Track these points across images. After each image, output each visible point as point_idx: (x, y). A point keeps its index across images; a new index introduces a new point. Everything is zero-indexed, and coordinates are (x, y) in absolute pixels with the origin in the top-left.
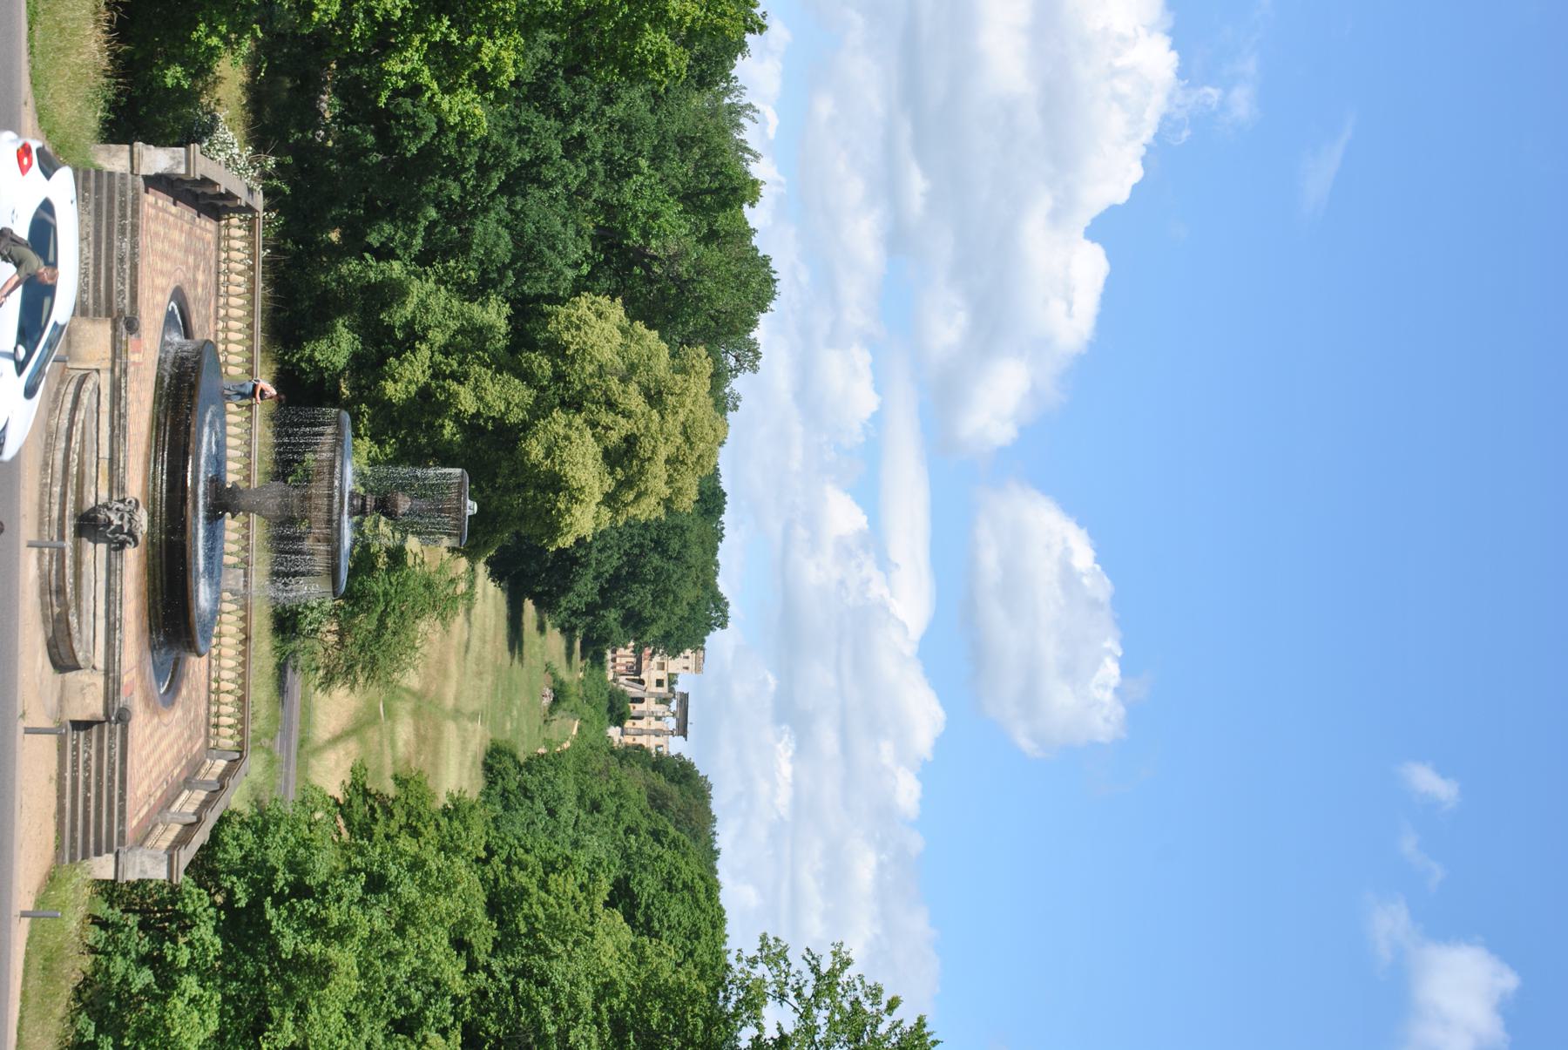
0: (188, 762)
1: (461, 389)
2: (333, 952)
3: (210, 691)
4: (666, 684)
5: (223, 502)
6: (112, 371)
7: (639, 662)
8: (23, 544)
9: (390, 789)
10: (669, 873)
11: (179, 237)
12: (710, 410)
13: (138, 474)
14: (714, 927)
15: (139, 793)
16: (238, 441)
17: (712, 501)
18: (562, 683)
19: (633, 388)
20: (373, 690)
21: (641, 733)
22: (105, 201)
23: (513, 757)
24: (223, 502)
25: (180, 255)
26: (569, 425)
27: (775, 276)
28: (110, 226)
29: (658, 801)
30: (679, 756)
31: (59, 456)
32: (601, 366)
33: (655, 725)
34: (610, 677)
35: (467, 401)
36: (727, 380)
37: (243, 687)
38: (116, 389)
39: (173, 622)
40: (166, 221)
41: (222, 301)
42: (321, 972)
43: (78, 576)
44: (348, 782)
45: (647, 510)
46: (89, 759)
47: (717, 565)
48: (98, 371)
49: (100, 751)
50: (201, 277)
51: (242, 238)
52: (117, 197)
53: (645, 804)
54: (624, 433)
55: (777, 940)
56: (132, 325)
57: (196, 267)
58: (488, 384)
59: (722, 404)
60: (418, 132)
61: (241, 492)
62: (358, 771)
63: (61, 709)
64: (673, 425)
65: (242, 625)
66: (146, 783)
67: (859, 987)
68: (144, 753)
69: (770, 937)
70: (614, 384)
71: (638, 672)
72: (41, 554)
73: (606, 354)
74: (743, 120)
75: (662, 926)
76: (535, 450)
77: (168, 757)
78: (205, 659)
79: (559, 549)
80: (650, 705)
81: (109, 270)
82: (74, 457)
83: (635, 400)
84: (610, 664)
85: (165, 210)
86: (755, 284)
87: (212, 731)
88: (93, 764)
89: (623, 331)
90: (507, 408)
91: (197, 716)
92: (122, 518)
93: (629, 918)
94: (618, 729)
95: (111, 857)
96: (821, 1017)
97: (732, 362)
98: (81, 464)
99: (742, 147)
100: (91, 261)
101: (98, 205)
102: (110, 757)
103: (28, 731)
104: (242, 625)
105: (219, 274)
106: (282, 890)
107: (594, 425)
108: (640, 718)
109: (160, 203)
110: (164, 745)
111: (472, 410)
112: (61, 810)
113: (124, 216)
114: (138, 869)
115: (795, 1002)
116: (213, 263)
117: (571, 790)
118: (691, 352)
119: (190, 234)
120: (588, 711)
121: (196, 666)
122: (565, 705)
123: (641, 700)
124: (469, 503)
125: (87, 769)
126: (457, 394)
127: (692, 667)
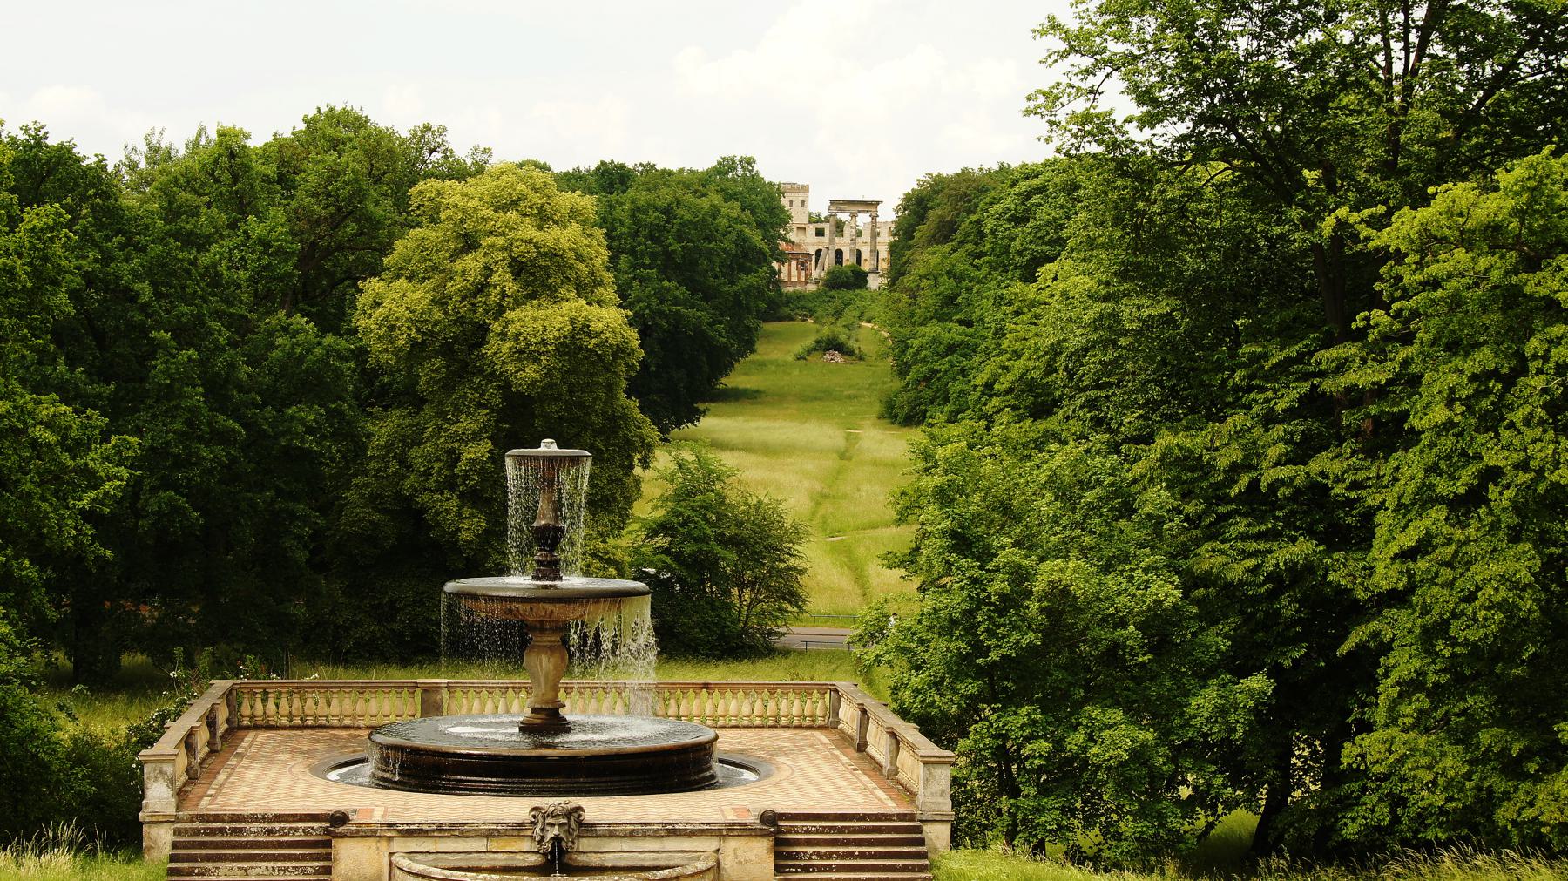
0: (838, 747)
1: (466, 456)
2: (1038, 587)
4: (820, 226)
7: (795, 256)
10: (1009, 221)
15: (860, 800)
17: (611, 179)
18: (819, 342)
21: (875, 253)
24: (549, 721)
26: (503, 336)
27: (324, 110)
29: (945, 232)
33: (866, 237)
34: (812, 288)
38: (410, 833)
39: (680, 768)
42: (1060, 597)
44: (903, 572)
46: (818, 854)
47: (681, 170)
48: (391, 854)
49: (809, 843)
51: (303, 700)
52: (199, 839)
53: (947, 248)
56: (340, 819)
58: (459, 428)
60: (176, 510)
62: (892, 560)
66: (849, 792)
70: (454, 287)
77: (827, 769)
79: (641, 346)
80: (844, 243)
81: (281, 845)
83: (471, 263)
84: (799, 288)
85: (222, 786)
86: (335, 131)
90: (485, 407)
92: (552, 825)
94: (870, 278)
95: (927, 828)
97: (436, 156)
100: (271, 864)
102: (817, 832)
106: (969, 644)
107: (501, 310)
108: (859, 253)
109: (211, 791)
110: (813, 774)
111: (489, 445)
113: (222, 831)
114: (940, 800)
115: (1101, 75)
116: (290, 733)
117: (933, 329)
118: (414, 202)
119: (253, 758)
120: (849, 315)
121: (727, 742)
122: (843, 338)
123: (839, 253)
125: (829, 856)
127: (801, 197)
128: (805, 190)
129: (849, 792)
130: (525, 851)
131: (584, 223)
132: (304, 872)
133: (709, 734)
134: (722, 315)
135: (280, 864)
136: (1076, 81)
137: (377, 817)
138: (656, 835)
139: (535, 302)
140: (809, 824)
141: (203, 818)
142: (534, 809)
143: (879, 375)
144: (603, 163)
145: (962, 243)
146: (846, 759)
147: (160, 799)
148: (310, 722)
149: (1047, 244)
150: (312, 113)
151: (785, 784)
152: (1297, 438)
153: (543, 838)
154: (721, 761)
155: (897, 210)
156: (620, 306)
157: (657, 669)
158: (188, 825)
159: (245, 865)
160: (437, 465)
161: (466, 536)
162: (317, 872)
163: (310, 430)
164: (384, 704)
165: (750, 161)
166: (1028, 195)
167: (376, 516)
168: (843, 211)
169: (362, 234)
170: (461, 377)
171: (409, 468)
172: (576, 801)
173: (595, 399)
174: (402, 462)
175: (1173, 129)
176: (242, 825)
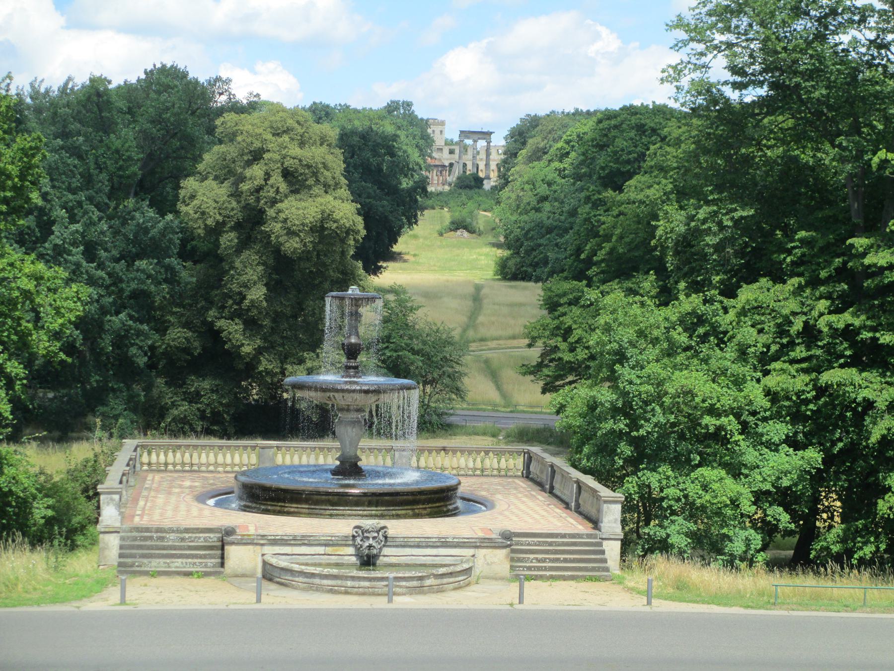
1: (249, 297)
3: (166, 471)
5: (350, 468)
6: (263, 545)
8: (390, 606)
11: (161, 499)
13: (341, 526)
14: (636, 114)
15: (559, 524)
16: (298, 459)
19: (248, 173)
20: (467, 359)
21: (487, 165)
22: (141, 552)
23: (507, 259)
24: (350, 468)
25: (173, 499)
27: (159, 65)
30: (506, 138)
31: (325, 582)
32: (232, 195)
33: (483, 155)
35: (257, 293)
36: (237, 102)
37: (478, 452)
39: (437, 501)
40: (151, 508)
41: (220, 469)
43: (408, 566)
44: (532, 377)
45: (336, 163)
46: (536, 559)
47: (364, 109)
50: (187, 483)
52: (137, 543)
54: (281, 179)
55: (663, 71)
56: (230, 532)
57: (181, 487)
59: (253, 107)
61: (342, 455)
63: (502, 579)
64: (273, 143)
65: (434, 453)
66: (551, 519)
67: (697, 11)
68: (531, 521)
69: (661, 75)
71: (444, 166)
72: (395, 594)
74: (42, 90)
75: (634, 152)
76: (292, 245)
77: (531, 504)
78: (462, 479)
80: (468, 159)
81: (190, 548)
82: (326, 571)
83: (257, 171)
85: (143, 509)
86: (166, 81)
87: (170, 467)
88: (540, 556)
89: (204, 179)
91: (500, 484)
93: (630, 175)
94: (485, 182)
95: (605, 543)
96: (719, 38)
98: (329, 565)
99: (63, 90)
100: (184, 560)
101: (144, 556)
102: (536, 545)
103: (521, 601)
104: (434, 453)
105: (192, 470)
107: (273, 202)
109: (138, 512)
112: (572, 578)
113: (151, 538)
114: (614, 525)
115: (710, 56)
116: (176, 475)
119: (157, 490)
121: (466, 486)
122: (468, 220)
123: (465, 165)
124: (350, 292)
126: (252, 301)
128: (442, 123)
129: (551, 519)
131: (329, 145)
132: (206, 566)
133: (453, 482)
134: (398, 206)
135: (190, 560)
136: (693, 60)
137: (252, 531)
139: (298, 196)
140: (530, 539)
141: (138, 529)
142: (356, 527)
144: (314, 103)
146: (542, 497)
149: (621, 164)
150: (149, 68)
151: (506, 513)
154: (464, 499)
156: (352, 201)
157: (418, 438)
158: (129, 534)
160: (230, 302)
163: (149, 276)
164: (239, 458)
165: (409, 105)
168: (468, 138)
169: (182, 148)
170: (246, 244)
172: (383, 523)
173: (333, 261)
174: (206, 300)
175: (751, 95)
176: (164, 535)
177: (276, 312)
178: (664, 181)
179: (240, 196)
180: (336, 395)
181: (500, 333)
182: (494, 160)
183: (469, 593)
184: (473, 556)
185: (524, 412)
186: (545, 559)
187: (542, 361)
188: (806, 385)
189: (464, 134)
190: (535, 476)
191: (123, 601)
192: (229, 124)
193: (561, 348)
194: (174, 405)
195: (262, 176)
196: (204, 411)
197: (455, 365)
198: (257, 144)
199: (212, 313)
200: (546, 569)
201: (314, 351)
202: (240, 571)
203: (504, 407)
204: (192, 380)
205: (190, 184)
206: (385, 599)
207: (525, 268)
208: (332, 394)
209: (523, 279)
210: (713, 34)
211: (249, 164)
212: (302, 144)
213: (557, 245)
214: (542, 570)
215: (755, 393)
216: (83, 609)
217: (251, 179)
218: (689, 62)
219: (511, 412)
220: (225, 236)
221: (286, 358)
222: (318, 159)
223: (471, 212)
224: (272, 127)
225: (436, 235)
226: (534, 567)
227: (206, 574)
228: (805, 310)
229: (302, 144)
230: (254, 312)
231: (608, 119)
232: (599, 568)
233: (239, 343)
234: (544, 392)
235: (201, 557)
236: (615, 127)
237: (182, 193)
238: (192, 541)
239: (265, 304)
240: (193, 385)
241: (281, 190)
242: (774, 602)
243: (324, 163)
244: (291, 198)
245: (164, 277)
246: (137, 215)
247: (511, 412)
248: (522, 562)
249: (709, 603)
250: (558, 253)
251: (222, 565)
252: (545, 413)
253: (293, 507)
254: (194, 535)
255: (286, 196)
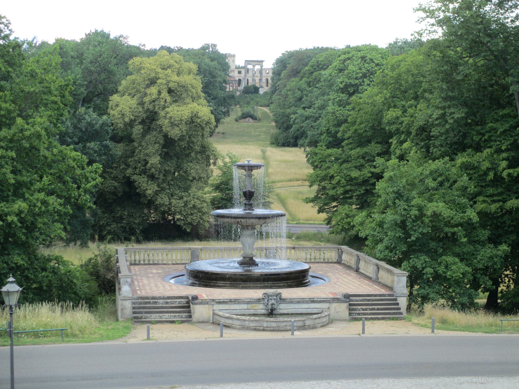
1: (150, 162)
8: (293, 337)
9: (315, 187)
12: (155, 57)
15: (371, 289)
22: (145, 310)
24: (249, 262)
27: (93, 31)
28: (154, 308)
33: (258, 74)
35: (155, 160)
39: (298, 279)
42: (435, 215)
46: (362, 309)
52: (142, 305)
53: (297, 79)
54: (167, 95)
56: (195, 298)
57: (152, 273)
64: (162, 74)
73: (133, 102)
76: (175, 133)
77: (349, 278)
81: (172, 307)
83: (153, 90)
86: (98, 39)
88: (364, 307)
92: (271, 299)
94: (260, 89)
100: (170, 315)
102: (360, 301)
103: (363, 333)
107: (164, 108)
112: (383, 319)
113: (149, 303)
122: (252, 112)
125: (366, 309)
126: (152, 164)
128: (234, 56)
130: (261, 308)
132: (182, 317)
133: (306, 266)
135: (172, 314)
136: (429, 28)
138: (307, 302)
139: (177, 104)
140: (357, 298)
141: (142, 298)
143: (270, 127)
145: (302, 77)
146: (354, 274)
147: (126, 292)
148: (151, 262)
151: (339, 283)
152: (511, 158)
153: (268, 304)
154: (313, 277)
155: (273, 64)
158: (137, 301)
159: (161, 315)
160: (139, 165)
161: (149, 192)
162: (186, 317)
163: (95, 152)
165: (215, 46)
166: (345, 61)
167: (116, 184)
168: (250, 64)
170: (148, 132)
171: (128, 166)
172: (279, 291)
174: (125, 164)
176: (156, 300)
177: (165, 170)
178: (385, 91)
179: (143, 104)
180: (242, 220)
181: (283, 178)
182: (265, 77)
183: (330, 329)
184: (329, 308)
185: (304, 224)
186: (367, 308)
187: (317, 195)
188: (497, 209)
189: (248, 62)
190: (346, 263)
191: (148, 338)
192: (137, 63)
193: (328, 187)
194: (108, 224)
195: (157, 93)
196: (125, 228)
197: (266, 198)
198: (153, 75)
199: (129, 171)
200: (368, 314)
201: (187, 192)
202: (201, 320)
203: (292, 221)
204: (119, 210)
205: (115, 98)
206: (290, 332)
207: (289, 140)
208: (239, 220)
209: (288, 146)
210: (440, 13)
211: (148, 86)
212: (178, 74)
213: (312, 126)
214: (366, 315)
215: (472, 214)
216: (128, 342)
217: (150, 95)
218: (426, 30)
219: (297, 224)
220: (136, 127)
221: (172, 196)
222: (189, 82)
223: (253, 108)
224: (161, 65)
225: (234, 121)
226: (361, 313)
227: (183, 322)
228: (494, 167)
229: (178, 74)
230: (153, 170)
231: (344, 54)
232: (397, 313)
233: (144, 189)
234: (319, 211)
235: (178, 312)
236: (349, 59)
237: (111, 103)
238: (172, 304)
239: (159, 166)
240: (118, 213)
241: (168, 101)
242: (501, 330)
243: (191, 84)
244: (174, 105)
245: (103, 152)
246: (87, 117)
247: (297, 224)
248: (354, 310)
249: (464, 331)
250: (313, 131)
251: (190, 317)
252: (316, 224)
253: (221, 283)
254: (173, 300)
255: (171, 104)
